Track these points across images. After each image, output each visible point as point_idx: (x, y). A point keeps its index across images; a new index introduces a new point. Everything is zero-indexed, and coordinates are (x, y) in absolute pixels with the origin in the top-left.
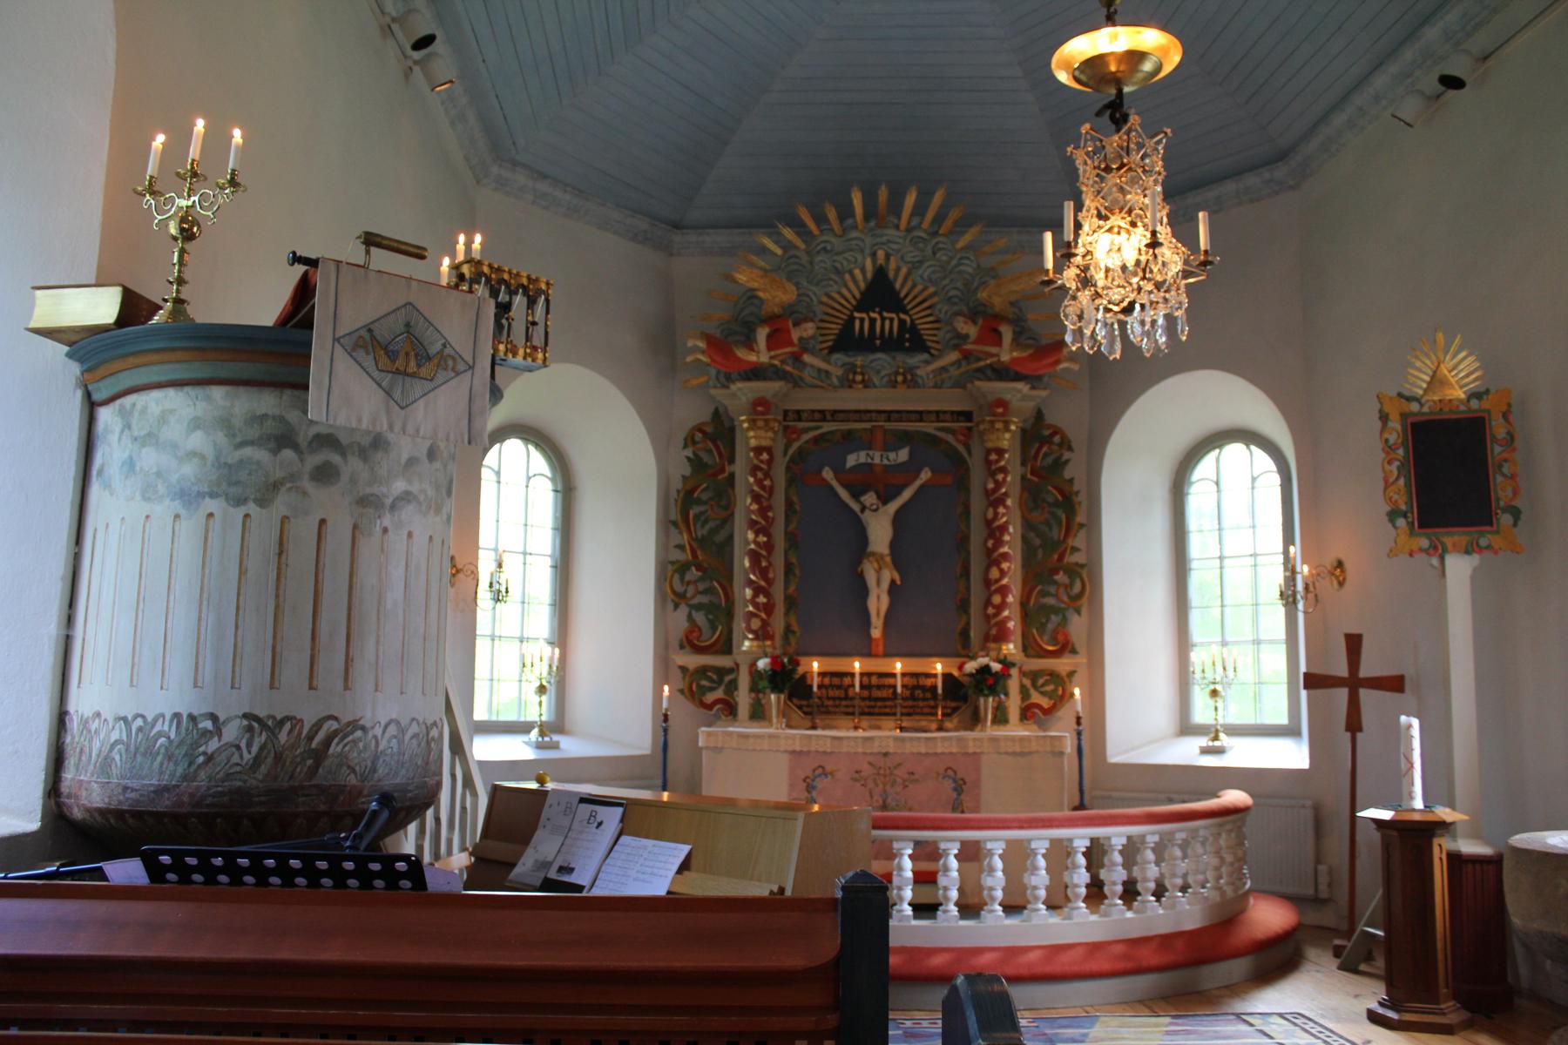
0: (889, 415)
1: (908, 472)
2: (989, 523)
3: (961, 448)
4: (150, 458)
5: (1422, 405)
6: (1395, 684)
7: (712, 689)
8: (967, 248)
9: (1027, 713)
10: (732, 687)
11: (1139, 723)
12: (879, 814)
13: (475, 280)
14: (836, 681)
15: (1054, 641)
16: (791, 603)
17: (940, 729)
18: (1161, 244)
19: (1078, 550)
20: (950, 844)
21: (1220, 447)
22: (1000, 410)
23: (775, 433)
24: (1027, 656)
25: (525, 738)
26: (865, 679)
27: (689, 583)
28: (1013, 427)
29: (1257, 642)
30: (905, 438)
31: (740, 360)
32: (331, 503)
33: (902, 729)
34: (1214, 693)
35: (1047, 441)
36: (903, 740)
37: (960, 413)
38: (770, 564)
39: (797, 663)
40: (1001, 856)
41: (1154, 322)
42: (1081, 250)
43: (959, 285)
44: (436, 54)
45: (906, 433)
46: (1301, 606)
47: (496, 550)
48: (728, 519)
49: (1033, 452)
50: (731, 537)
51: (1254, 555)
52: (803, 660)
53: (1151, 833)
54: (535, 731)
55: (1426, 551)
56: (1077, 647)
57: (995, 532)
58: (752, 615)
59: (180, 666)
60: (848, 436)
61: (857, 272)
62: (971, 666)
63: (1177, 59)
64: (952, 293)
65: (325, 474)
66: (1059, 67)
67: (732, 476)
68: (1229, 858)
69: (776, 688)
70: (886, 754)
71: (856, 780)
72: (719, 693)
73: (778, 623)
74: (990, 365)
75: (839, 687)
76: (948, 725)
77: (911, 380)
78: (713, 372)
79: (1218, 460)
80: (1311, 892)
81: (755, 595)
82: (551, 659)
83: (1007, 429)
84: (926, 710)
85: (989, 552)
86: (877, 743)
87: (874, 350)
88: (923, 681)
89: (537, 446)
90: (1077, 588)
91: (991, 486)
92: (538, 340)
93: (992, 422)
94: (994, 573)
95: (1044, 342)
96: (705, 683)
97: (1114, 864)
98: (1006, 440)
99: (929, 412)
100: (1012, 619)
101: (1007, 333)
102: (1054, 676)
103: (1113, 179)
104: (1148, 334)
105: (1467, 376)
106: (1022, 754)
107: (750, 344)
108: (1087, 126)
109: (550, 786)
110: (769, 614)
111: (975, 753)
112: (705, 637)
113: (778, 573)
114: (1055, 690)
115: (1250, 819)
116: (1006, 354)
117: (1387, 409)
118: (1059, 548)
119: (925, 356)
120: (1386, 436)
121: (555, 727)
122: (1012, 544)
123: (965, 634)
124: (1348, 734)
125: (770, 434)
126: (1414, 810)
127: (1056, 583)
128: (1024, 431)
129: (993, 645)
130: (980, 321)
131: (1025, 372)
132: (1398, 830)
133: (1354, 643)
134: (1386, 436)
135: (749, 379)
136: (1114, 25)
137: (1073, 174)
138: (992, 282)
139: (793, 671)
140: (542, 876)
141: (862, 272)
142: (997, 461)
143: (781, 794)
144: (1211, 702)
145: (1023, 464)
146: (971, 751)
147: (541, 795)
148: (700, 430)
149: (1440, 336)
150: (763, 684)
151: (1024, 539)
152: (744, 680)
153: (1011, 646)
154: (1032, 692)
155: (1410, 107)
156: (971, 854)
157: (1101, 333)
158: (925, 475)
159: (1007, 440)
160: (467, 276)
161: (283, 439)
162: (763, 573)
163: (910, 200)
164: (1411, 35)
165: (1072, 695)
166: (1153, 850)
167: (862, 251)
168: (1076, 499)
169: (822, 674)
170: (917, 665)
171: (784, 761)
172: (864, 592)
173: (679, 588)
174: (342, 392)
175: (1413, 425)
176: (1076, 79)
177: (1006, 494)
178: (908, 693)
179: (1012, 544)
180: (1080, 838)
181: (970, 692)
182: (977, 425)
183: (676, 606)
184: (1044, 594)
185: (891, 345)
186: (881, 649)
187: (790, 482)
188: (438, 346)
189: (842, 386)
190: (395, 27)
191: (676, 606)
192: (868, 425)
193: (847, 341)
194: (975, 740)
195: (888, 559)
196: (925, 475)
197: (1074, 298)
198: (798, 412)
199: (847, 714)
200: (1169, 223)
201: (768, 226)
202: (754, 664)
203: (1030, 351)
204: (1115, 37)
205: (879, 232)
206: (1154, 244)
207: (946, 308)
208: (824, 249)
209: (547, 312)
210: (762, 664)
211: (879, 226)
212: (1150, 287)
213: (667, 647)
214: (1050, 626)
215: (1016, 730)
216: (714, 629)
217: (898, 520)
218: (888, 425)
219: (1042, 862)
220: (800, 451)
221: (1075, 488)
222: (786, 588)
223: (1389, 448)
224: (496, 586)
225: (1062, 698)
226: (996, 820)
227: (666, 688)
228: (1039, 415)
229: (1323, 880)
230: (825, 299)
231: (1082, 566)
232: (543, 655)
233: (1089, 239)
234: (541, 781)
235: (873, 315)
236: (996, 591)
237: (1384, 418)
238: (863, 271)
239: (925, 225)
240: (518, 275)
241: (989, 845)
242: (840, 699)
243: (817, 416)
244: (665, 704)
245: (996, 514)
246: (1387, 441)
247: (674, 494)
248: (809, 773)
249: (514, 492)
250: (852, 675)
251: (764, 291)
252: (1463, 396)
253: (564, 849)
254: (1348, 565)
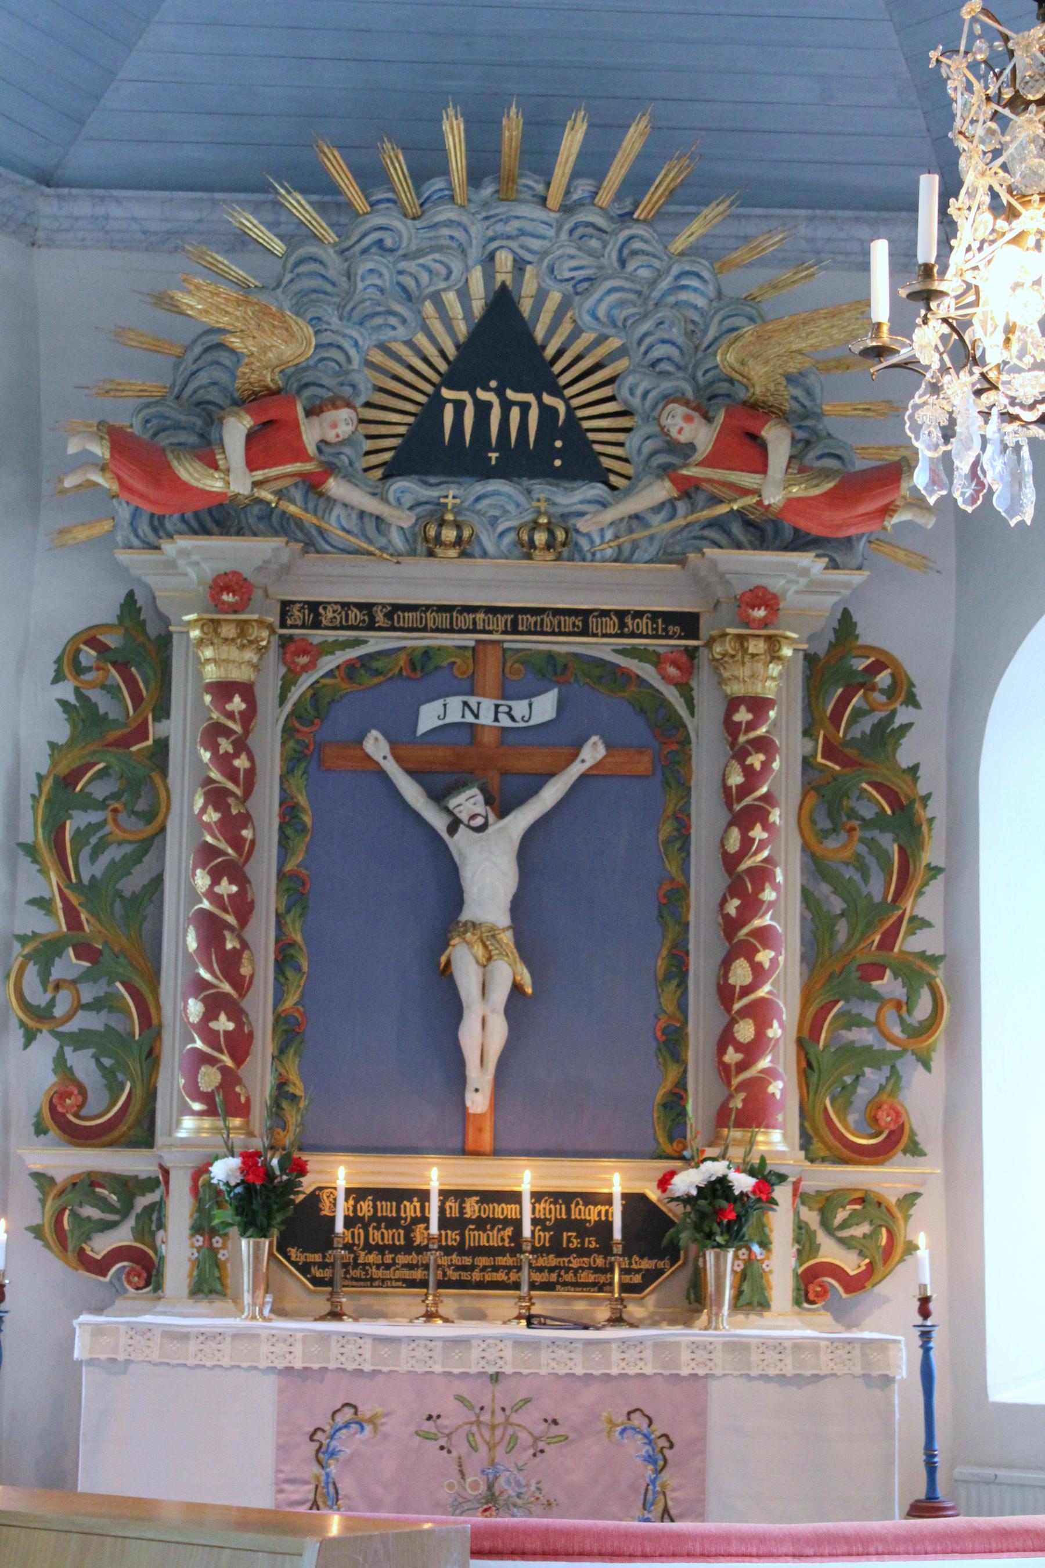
0: (515, 618)
1: (559, 741)
2: (730, 862)
3: (671, 694)
7: (107, 1226)
8: (692, 252)
9: (810, 1286)
10: (153, 1220)
12: (479, 1520)
14: (387, 1209)
16: (289, 1033)
17: (617, 1320)
19: (925, 924)
22: (761, 613)
23: (261, 651)
26: (452, 1204)
28: (787, 652)
30: (552, 670)
31: (186, 488)
33: (531, 1321)
35: (863, 682)
36: (534, 1345)
37: (670, 617)
42: (949, 284)
43: (676, 334)
45: (551, 657)
48: (152, 842)
50: (158, 881)
52: (314, 1161)
57: (744, 883)
60: (422, 662)
61: (450, 298)
62: (688, 1181)
67: (162, 746)
70: (496, 1378)
71: (427, 1436)
72: (123, 1236)
73: (259, 1079)
74: (740, 514)
75: (393, 1223)
76: (634, 1310)
77: (561, 541)
78: (124, 513)
81: (210, 1014)
83: (774, 657)
85: (731, 926)
86: (475, 1354)
87: (487, 473)
90: (923, 1009)
91: (736, 779)
93: (741, 639)
95: (860, 465)
96: (89, 1211)
101: (778, 440)
106: (798, 1380)
107: (208, 453)
110: (239, 1058)
111: (694, 1376)
112: (93, 1105)
113: (261, 965)
114: (873, 1235)
116: (775, 489)
118: (886, 920)
119: (598, 490)
122: (781, 908)
123: (674, 1104)
125: (250, 655)
128: (810, 659)
129: (736, 1134)
130: (721, 417)
131: (815, 529)
135: (206, 532)
137: (939, 110)
139: (291, 1186)
141: (454, 316)
142: (751, 726)
143: (260, 1496)
148: (93, 642)
150: (224, 1215)
152: (180, 1208)
154: (822, 1237)
157: (994, 470)
158: (593, 752)
159: (775, 679)
162: (230, 965)
163: (572, 141)
165: (911, 1248)
168: (925, 814)
171: (267, 1389)
172: (451, 1009)
173: (37, 997)
177: (767, 798)
179: (781, 908)
182: (710, 644)
183: (30, 1037)
184: (855, 1021)
185: (522, 462)
186: (487, 1139)
187: (293, 762)
189: (413, 553)
191: (30, 1037)
192: (468, 640)
193: (425, 451)
195: (507, 938)
197: (935, 389)
198: (313, 607)
199: (411, 1283)
201: (252, 186)
202: (204, 1169)
205: (502, 209)
208: (380, 243)
210: (224, 1170)
211: (503, 196)
214: (863, 1092)
215: (784, 1324)
217: (529, 851)
220: (315, 692)
221: (922, 789)
222: (279, 997)
225: (888, 1252)
226: (743, 1538)
228: (846, 625)
230: (378, 357)
231: (935, 960)
233: (978, 259)
235: (482, 395)
236: (744, 1013)
238: (464, 294)
239: (604, 198)
242: (394, 1249)
243: (356, 616)
245: (747, 842)
247: (30, 785)
250: (424, 1195)
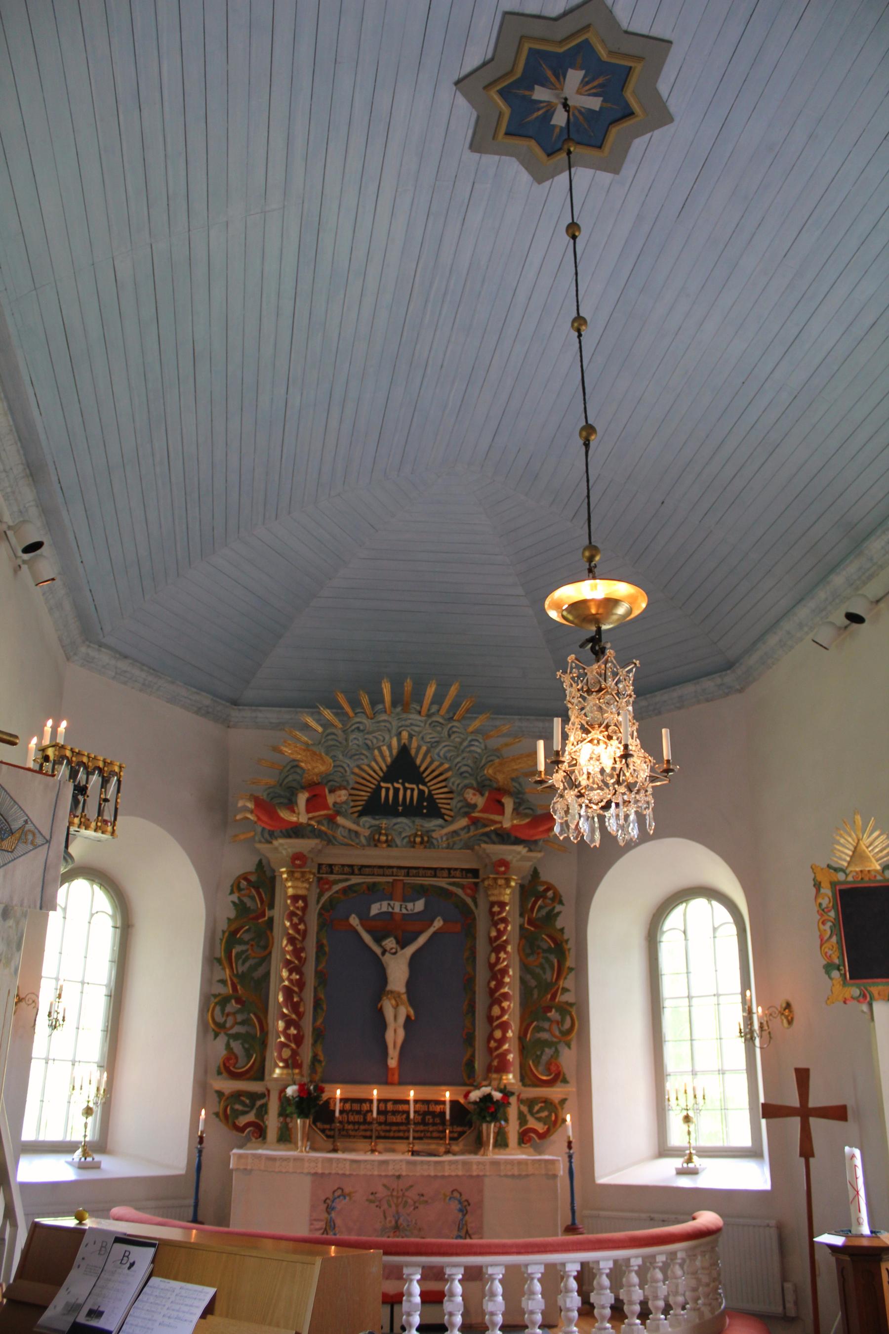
1: (425, 919)
2: (492, 966)
3: (469, 901)
5: (847, 875)
6: (839, 1113)
7: (244, 1113)
8: (476, 732)
9: (524, 1138)
10: (263, 1111)
11: (625, 1158)
13: (58, 762)
14: (356, 1107)
15: (548, 1071)
16: (318, 1035)
17: (447, 1152)
18: (632, 756)
20: (455, 1269)
21: (686, 901)
22: (503, 869)
23: (310, 883)
24: (524, 1085)
25: (69, 1158)
26: (382, 1105)
27: (228, 1015)
28: (513, 884)
29: (722, 1072)
30: (421, 891)
34: (687, 1119)
35: (542, 895)
36: (414, 1163)
37: (468, 871)
38: (301, 999)
39: (322, 1090)
40: (501, 1281)
41: (627, 817)
42: (566, 758)
43: (470, 762)
44: (41, 555)
45: (422, 886)
46: (757, 1042)
47: (57, 979)
48: (266, 958)
49: (530, 906)
51: (717, 995)
52: (327, 1087)
53: (635, 1256)
54: (79, 1152)
55: (857, 999)
56: (568, 1079)
57: (497, 975)
58: (283, 1045)
60: (372, 888)
61: (385, 748)
62: (475, 1095)
63: (644, 605)
64: (464, 769)
66: (550, 607)
67: (271, 920)
68: (705, 1279)
69: (303, 1114)
70: (399, 1177)
71: (371, 1201)
72: (251, 1117)
73: (306, 1054)
74: (495, 831)
75: (358, 1112)
76: (455, 1148)
78: (259, 829)
79: (685, 915)
80: (780, 1309)
81: (287, 1027)
82: (99, 1082)
83: (508, 885)
84: (435, 1134)
86: (391, 1167)
87: (397, 814)
88: (432, 1108)
89: (101, 885)
90: (567, 1024)
92: (108, 816)
94: (496, 1011)
96: (238, 1107)
97: (602, 1288)
98: (507, 895)
99: (442, 869)
101: (509, 803)
102: (547, 1103)
103: (593, 700)
104: (622, 827)
105: (881, 851)
106: (519, 1176)
107: (291, 806)
108: (573, 656)
109: (89, 1223)
111: (478, 1176)
112: (239, 1064)
114: (549, 1116)
115: (722, 1238)
116: (508, 821)
117: (819, 878)
118: (551, 988)
119: (440, 821)
120: (820, 900)
121: (99, 1146)
122: (511, 984)
123: (470, 1063)
124: (803, 1160)
125: (306, 885)
126: (862, 1236)
127: (549, 1019)
128: (522, 887)
129: (494, 1076)
130: (487, 794)
132: (851, 1255)
133: (803, 1076)
134: (820, 900)
135: (289, 836)
136: (594, 578)
138: (497, 761)
139: (318, 1097)
140: (71, 1320)
142: (500, 913)
144: (685, 1127)
145: (522, 915)
146: (475, 1174)
147: (78, 1234)
148: (246, 879)
149: (858, 818)
151: (522, 981)
153: (511, 1076)
154: (529, 1117)
155: (825, 635)
156: (474, 1276)
157: (584, 826)
158: (438, 923)
160: (52, 758)
162: (295, 1007)
163: (431, 690)
164: (823, 579)
165: (564, 1120)
166: (637, 1273)
167: (389, 731)
168: (567, 947)
169: (344, 1100)
170: (429, 1093)
173: (220, 1019)
175: (840, 891)
176: (564, 617)
177: (506, 941)
178: (419, 1118)
179: (511, 984)
180: (572, 1262)
181: (475, 1118)
182: (483, 881)
183: (216, 1035)
184: (539, 1029)
185: (412, 811)
186: (396, 1077)
187: (322, 926)
188: (21, 822)
189: (369, 845)
190: (9, 533)
192: (390, 879)
193: (374, 806)
194: (479, 1163)
195: (404, 997)
196: (438, 923)
197: (562, 796)
198: (331, 866)
199: (365, 1137)
200: (638, 737)
201: (310, 706)
202: (283, 1091)
203: (527, 820)
204: (595, 587)
205: (404, 716)
206: (626, 755)
207: (458, 781)
208: (358, 728)
209: (118, 791)
210: (291, 1091)
212: (622, 789)
213: (206, 1072)
214: (545, 1058)
215: (516, 1154)
216: (249, 1057)
217: (413, 962)
218: (408, 880)
219: (538, 1287)
220: (331, 899)
221: (566, 937)
223: (822, 911)
224: (54, 1015)
227: (203, 1112)
228: (535, 873)
229: (790, 1298)
230: (357, 770)
231: (571, 1005)
232: (91, 1077)
234: (80, 1218)
235: (396, 785)
237: (818, 885)
238: (390, 747)
239: (443, 711)
240: (95, 758)
241: (490, 1271)
242: (359, 1123)
243: (347, 869)
244: (201, 1128)
245: (498, 959)
246: (820, 904)
247: (219, 934)
248: (330, 1195)
249: (78, 928)
250: (371, 1101)
251: (305, 762)
252: (878, 868)
253: (96, 1290)
254: (795, 1006)
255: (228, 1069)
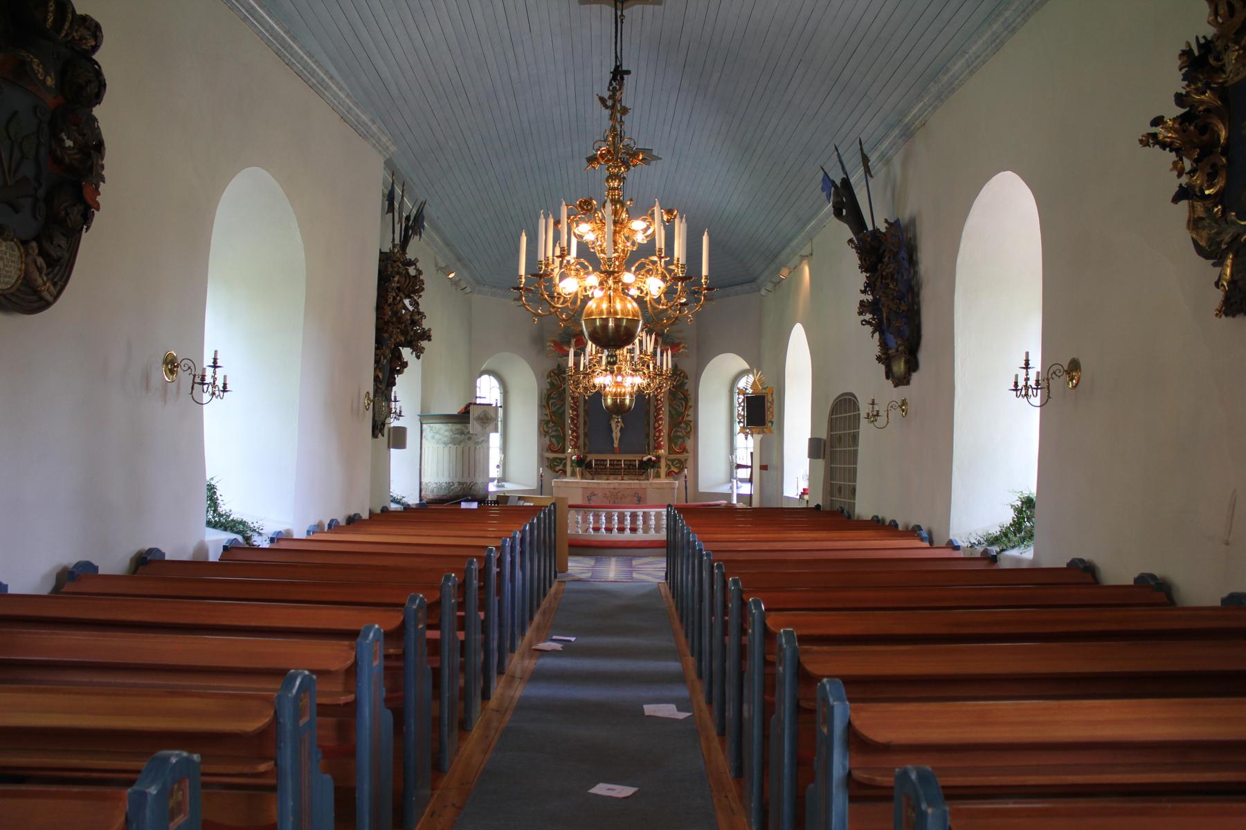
4: (437, 436)
10: (565, 465)
16: (586, 435)
32: (470, 444)
59: (446, 474)
65: (469, 439)
100: (664, 441)
102: (680, 461)
118: (682, 414)
143: (220, 509)
161: (462, 433)
162: (575, 425)
170: (630, 457)
171: (581, 491)
174: (474, 427)
215: (663, 480)
255: (550, 449)
